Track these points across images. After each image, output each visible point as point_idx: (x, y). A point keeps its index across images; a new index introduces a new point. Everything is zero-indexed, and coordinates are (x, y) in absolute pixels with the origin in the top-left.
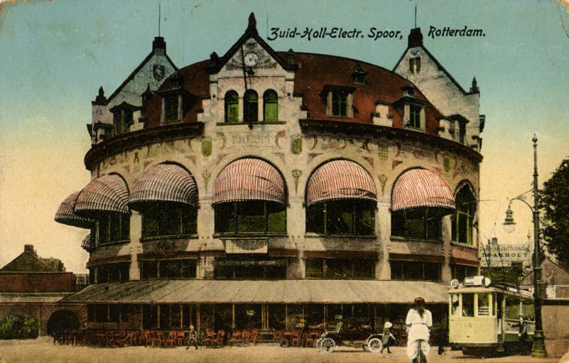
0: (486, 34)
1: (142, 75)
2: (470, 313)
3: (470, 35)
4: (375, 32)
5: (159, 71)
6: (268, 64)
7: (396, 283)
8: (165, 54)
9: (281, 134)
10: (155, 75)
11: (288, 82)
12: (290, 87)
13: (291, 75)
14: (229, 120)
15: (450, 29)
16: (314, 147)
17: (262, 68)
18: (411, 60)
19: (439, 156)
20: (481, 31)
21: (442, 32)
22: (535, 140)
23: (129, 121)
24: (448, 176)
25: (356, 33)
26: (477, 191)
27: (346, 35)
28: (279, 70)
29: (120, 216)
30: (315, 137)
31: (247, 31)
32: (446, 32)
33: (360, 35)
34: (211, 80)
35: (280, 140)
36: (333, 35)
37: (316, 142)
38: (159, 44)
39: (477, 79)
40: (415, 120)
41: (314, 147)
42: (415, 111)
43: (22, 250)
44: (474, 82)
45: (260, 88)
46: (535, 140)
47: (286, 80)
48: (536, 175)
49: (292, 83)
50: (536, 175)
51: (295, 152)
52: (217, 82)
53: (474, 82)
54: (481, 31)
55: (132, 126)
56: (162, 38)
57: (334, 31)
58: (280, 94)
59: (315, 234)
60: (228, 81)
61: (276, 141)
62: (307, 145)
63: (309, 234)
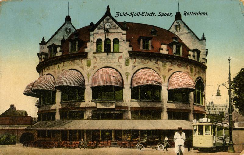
0: (208, 14)
1: (61, 32)
2: (202, 133)
3: (202, 15)
4: (161, 14)
5: (68, 31)
6: (115, 27)
7: (170, 121)
8: (71, 23)
9: (121, 57)
10: (67, 32)
11: (123, 35)
12: (124, 37)
13: (125, 32)
14: (98, 51)
15: (193, 13)
16: (135, 63)
17: (112, 29)
18: (176, 26)
19: (188, 67)
20: (206, 13)
21: (190, 14)
22: (229, 60)
23: (55, 52)
24: (192, 75)
25: (153, 14)
26: (204, 82)
27: (149, 15)
28: (120, 30)
29: (52, 92)
30: (135, 58)
31: (106, 13)
32: (191, 14)
33: (154, 15)
34: (90, 34)
35: (120, 60)
36: (143, 15)
37: (136, 61)
38: (68, 19)
39: (204, 34)
40: (178, 51)
41: (135, 63)
42: (178, 47)
43: (9, 107)
44: (203, 35)
45: (112, 37)
46: (229, 60)
47: (123, 34)
48: (230, 75)
49: (125, 35)
50: (230, 75)
51: (126, 65)
52: (93, 35)
53: (203, 35)
54: (206, 13)
55: (56, 54)
56: (70, 16)
57: (143, 13)
58: (120, 40)
59: (135, 100)
60: (98, 35)
61: (119, 60)
62: (131, 62)
63: (132, 100)
